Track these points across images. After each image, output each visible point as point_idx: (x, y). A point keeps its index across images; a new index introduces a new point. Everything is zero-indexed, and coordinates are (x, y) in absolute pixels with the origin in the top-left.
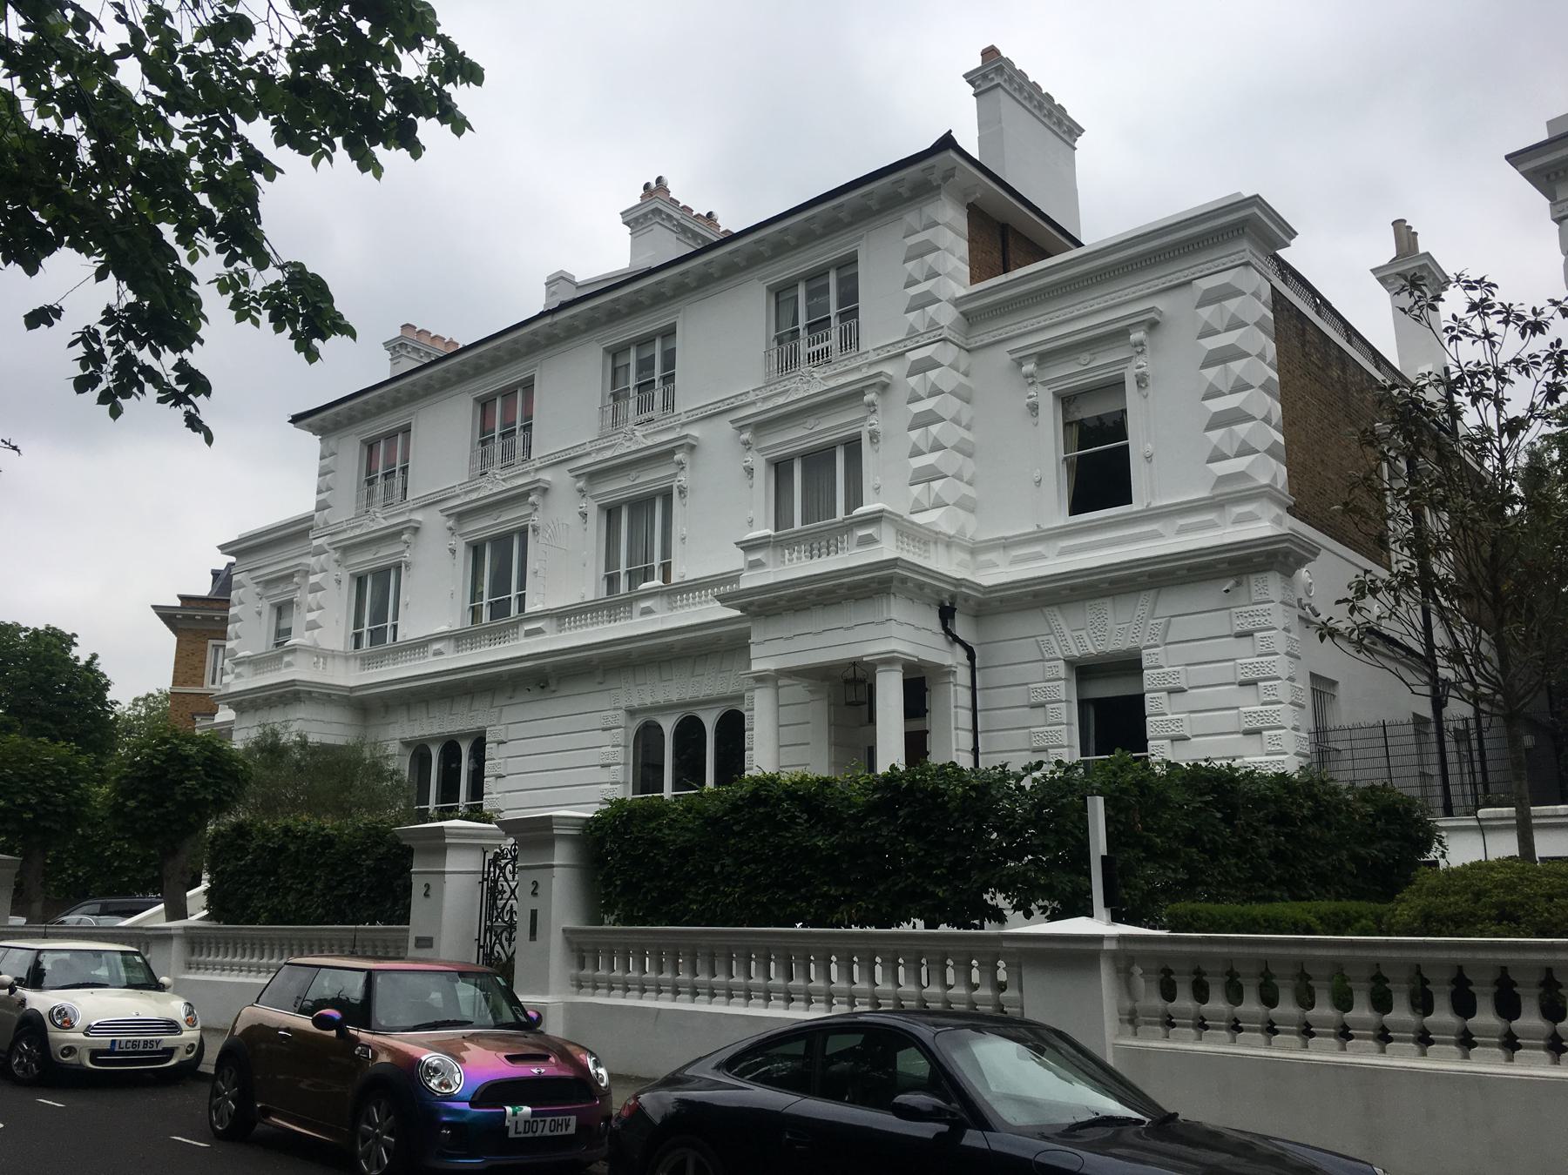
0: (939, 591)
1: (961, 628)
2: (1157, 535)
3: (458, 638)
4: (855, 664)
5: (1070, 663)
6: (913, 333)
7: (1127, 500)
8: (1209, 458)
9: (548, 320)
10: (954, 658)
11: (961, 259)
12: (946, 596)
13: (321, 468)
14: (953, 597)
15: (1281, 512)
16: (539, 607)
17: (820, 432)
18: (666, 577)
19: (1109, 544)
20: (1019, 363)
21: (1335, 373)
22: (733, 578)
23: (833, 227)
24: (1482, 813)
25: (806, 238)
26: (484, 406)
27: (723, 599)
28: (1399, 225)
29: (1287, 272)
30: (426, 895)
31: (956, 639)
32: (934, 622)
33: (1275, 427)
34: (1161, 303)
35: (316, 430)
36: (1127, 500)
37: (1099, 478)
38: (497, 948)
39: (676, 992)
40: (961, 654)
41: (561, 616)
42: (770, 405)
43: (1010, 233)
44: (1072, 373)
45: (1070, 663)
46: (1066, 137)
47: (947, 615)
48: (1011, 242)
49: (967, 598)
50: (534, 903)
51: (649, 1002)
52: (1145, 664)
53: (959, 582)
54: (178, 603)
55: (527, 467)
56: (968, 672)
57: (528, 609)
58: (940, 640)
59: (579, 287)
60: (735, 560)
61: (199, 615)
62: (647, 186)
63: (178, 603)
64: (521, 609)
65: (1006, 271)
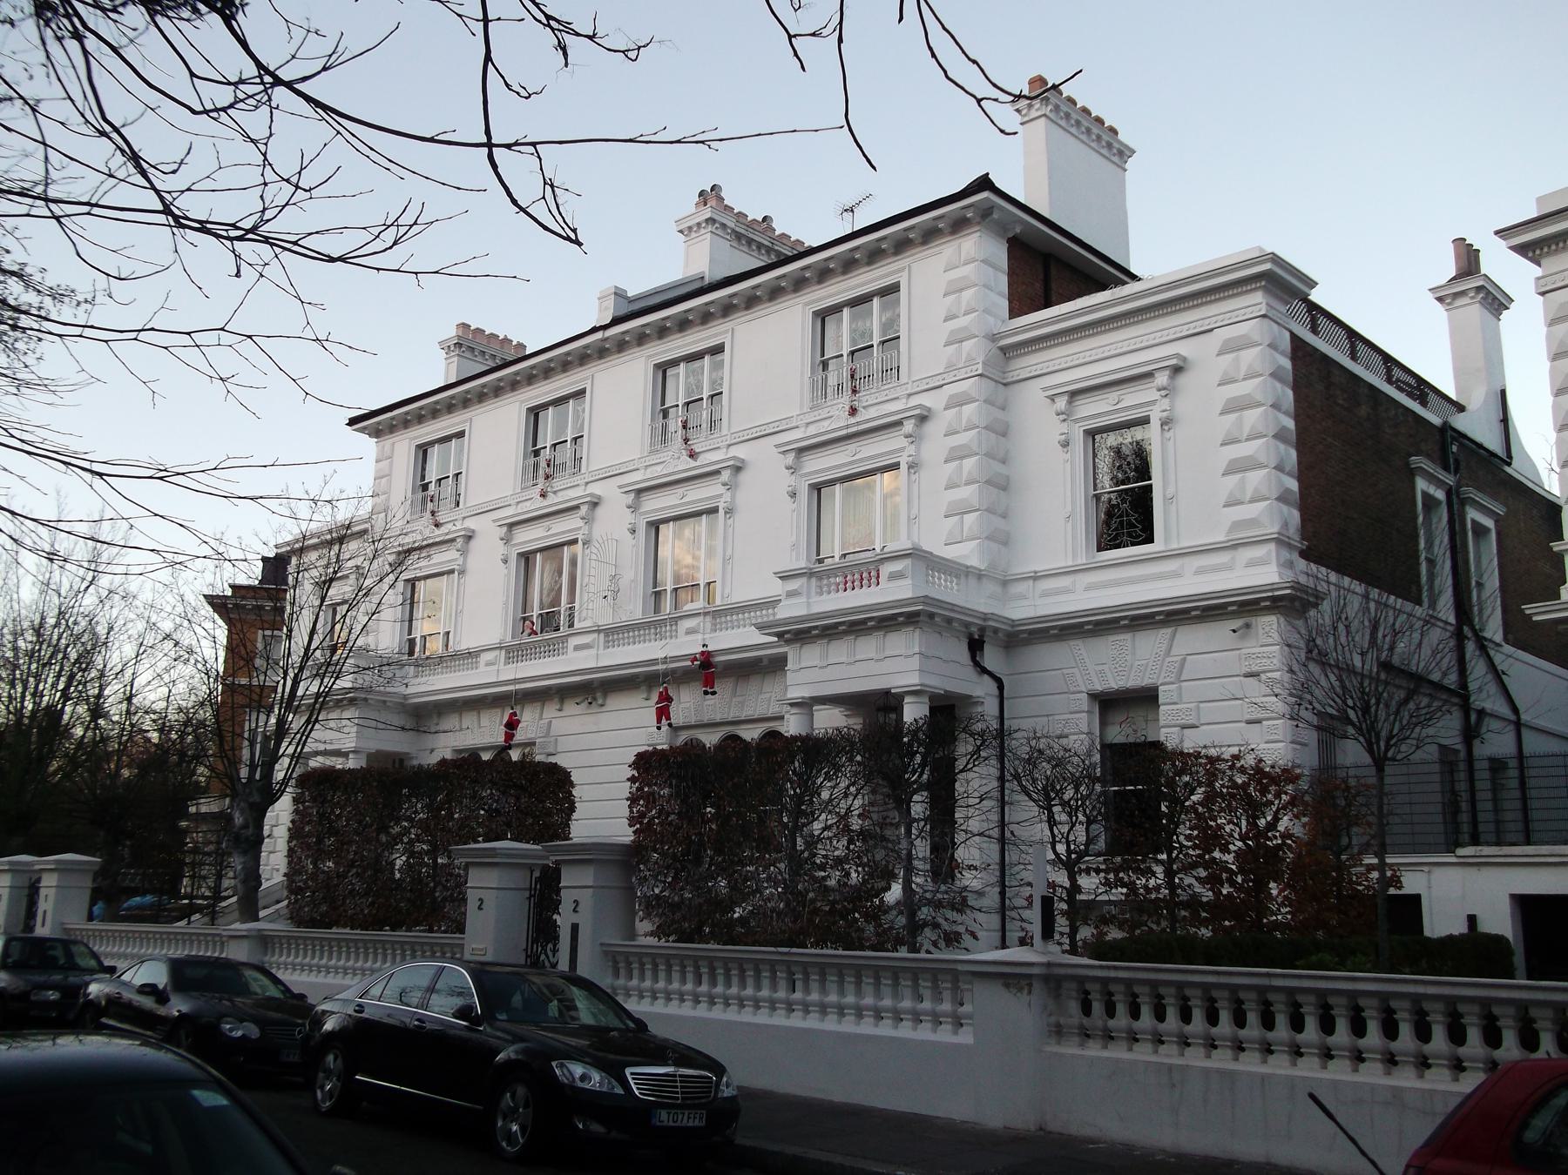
0: (967, 625)
1: (991, 658)
2: (1176, 575)
3: (513, 653)
4: (887, 693)
5: (1093, 696)
6: (951, 367)
7: (1150, 540)
8: (1229, 502)
9: (599, 335)
10: (982, 689)
11: (1000, 294)
12: (974, 629)
14: (982, 629)
15: (1295, 556)
16: (588, 623)
17: (861, 460)
18: (709, 598)
19: (1133, 580)
20: (1052, 398)
21: (1364, 411)
22: (773, 603)
23: (875, 255)
24: (1461, 851)
26: (527, 560)
27: (761, 627)
28: (1459, 242)
29: (1313, 308)
30: (480, 908)
31: (984, 671)
32: (963, 654)
33: (1289, 474)
34: (1183, 348)
35: (377, 433)
36: (1150, 540)
37: (1127, 517)
38: (543, 957)
39: (938, 1023)
40: (991, 686)
41: (612, 634)
42: (812, 430)
43: (1052, 267)
44: (1097, 409)
45: (1093, 696)
46: (1116, 159)
47: (975, 647)
48: (1053, 272)
49: (996, 631)
50: (575, 919)
51: (763, 1018)
52: (1161, 701)
53: (986, 617)
54: (229, 592)
55: (577, 480)
56: (996, 702)
57: (576, 625)
58: (969, 671)
59: (631, 301)
60: (777, 588)
61: (250, 603)
62: (702, 193)
63: (229, 592)
64: (571, 625)
65: (1048, 305)
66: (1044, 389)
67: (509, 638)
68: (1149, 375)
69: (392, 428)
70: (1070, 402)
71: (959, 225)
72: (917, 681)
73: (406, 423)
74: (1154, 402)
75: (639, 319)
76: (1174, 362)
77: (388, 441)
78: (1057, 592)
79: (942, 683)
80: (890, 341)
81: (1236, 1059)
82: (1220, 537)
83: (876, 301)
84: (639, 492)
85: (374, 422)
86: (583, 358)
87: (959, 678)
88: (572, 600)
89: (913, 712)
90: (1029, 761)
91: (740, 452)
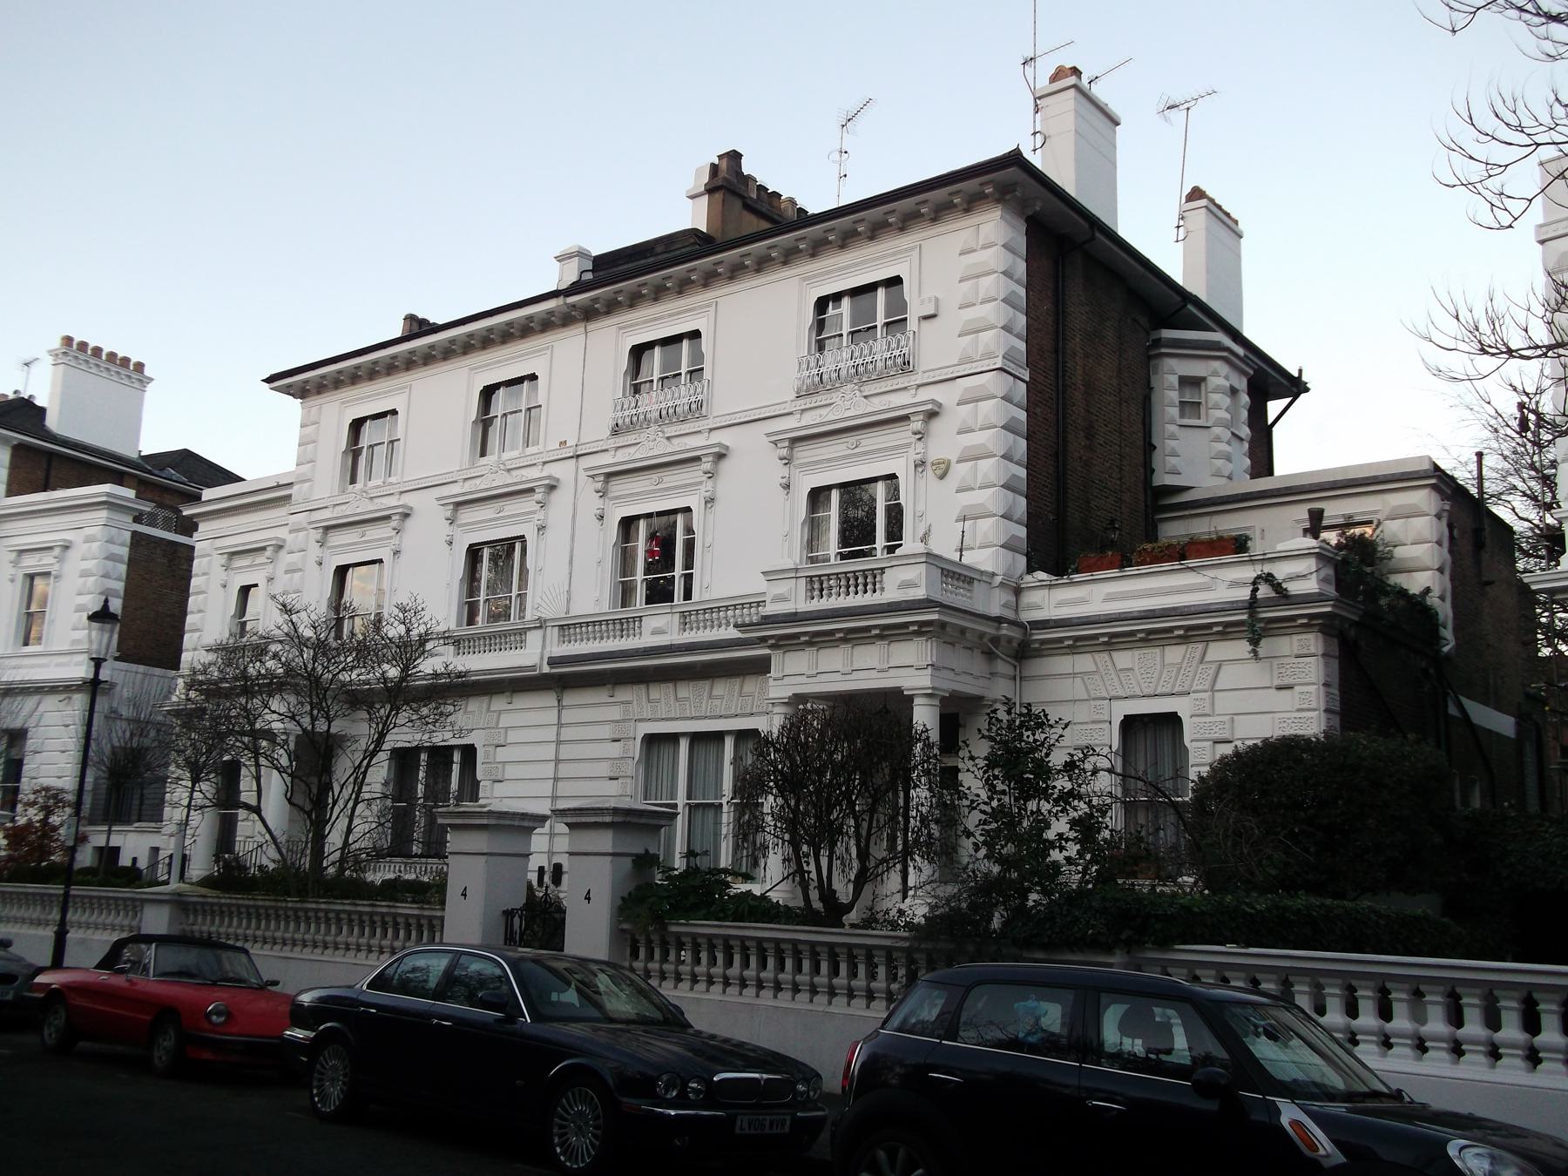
13: (301, 437)
25: (506, 335)
35: (301, 392)
57: (696, 596)
64: (688, 595)
66: (768, 435)
67: (453, 626)
68: (905, 418)
69: (321, 387)
70: (791, 448)
71: (972, 204)
72: (929, 684)
73: (337, 383)
74: (534, 512)
75: (618, 277)
76: (929, 407)
77: (315, 401)
78: (33, 666)
79: (950, 684)
80: (696, 373)
81: (830, 1003)
82: (66, 647)
83: (657, 350)
84: (327, 528)
85: (301, 382)
86: (527, 330)
87: (969, 677)
88: (689, 564)
89: (924, 716)
90: (222, 737)
91: (408, 499)
